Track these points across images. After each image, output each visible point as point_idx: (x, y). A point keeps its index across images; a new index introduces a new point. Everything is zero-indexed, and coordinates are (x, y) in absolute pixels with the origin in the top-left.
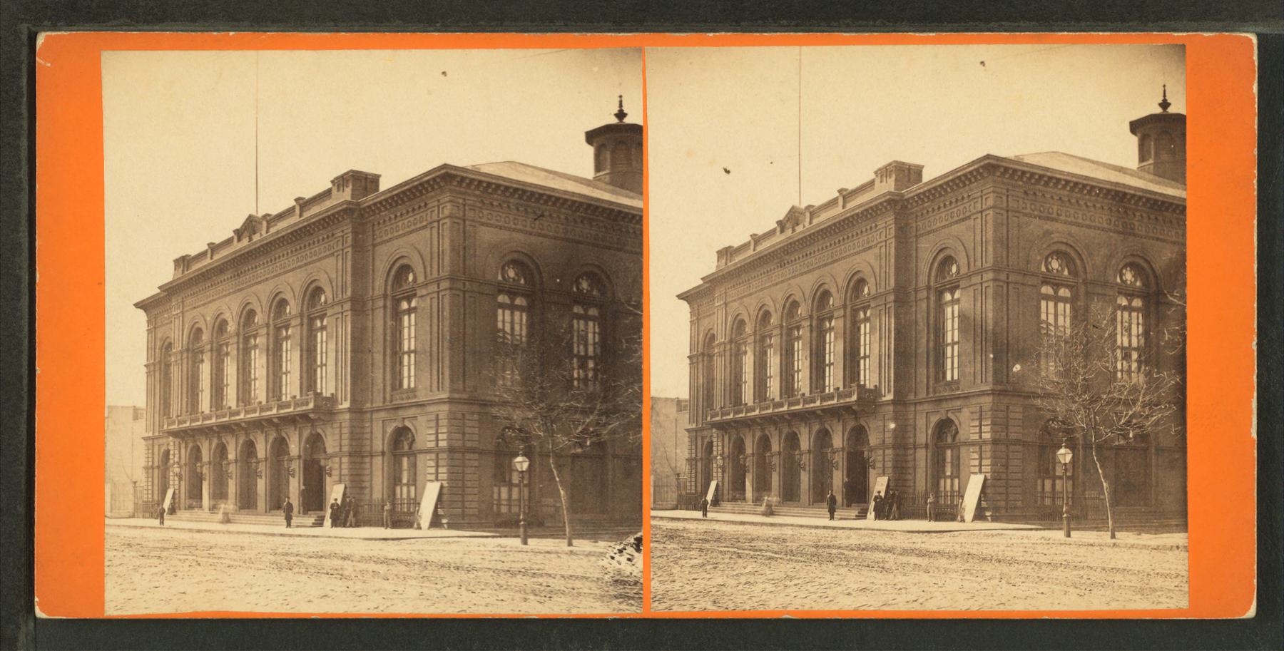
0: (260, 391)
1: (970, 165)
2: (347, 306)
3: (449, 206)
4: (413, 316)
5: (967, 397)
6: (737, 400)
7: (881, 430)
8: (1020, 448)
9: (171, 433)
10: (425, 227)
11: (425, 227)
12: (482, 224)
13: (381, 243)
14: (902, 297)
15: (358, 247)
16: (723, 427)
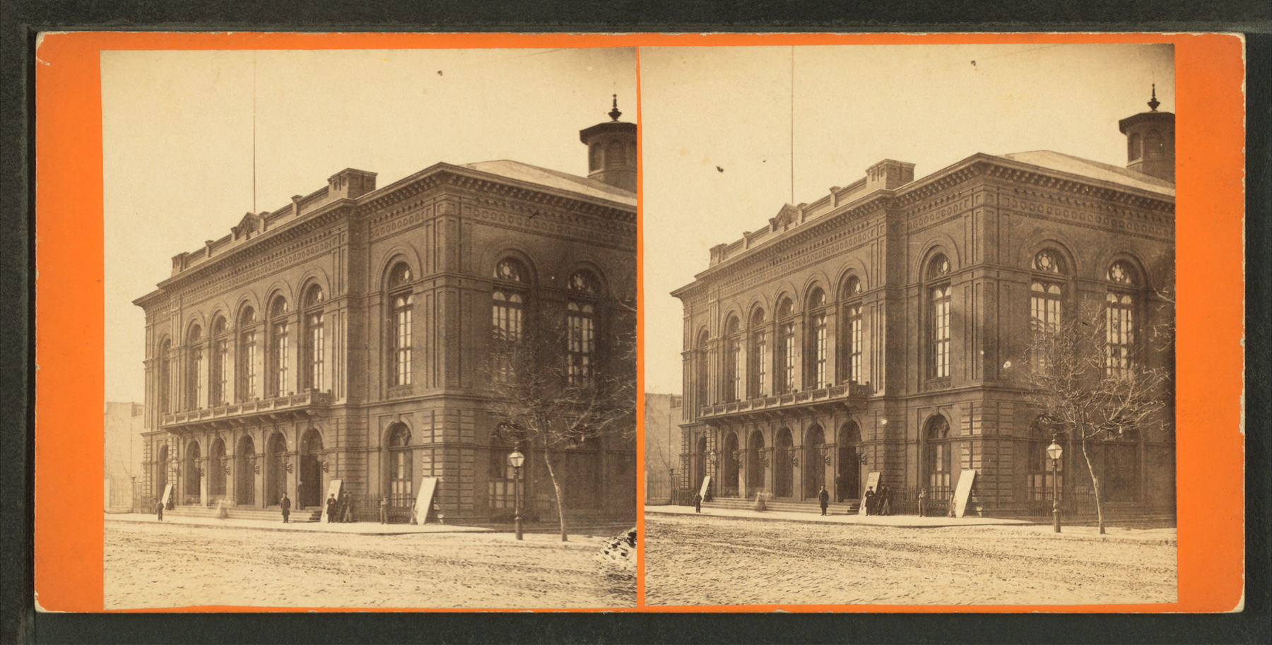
0: (257, 387)
1: (961, 163)
2: (344, 303)
3: (445, 204)
4: (409, 313)
5: (957, 393)
6: (730, 396)
7: (873, 426)
8: (1010, 444)
9: (173, 430)
10: (421, 225)
11: (421, 225)
12: (478, 222)
13: (377, 241)
14: (894, 294)
15: (355, 245)
16: (716, 423)
